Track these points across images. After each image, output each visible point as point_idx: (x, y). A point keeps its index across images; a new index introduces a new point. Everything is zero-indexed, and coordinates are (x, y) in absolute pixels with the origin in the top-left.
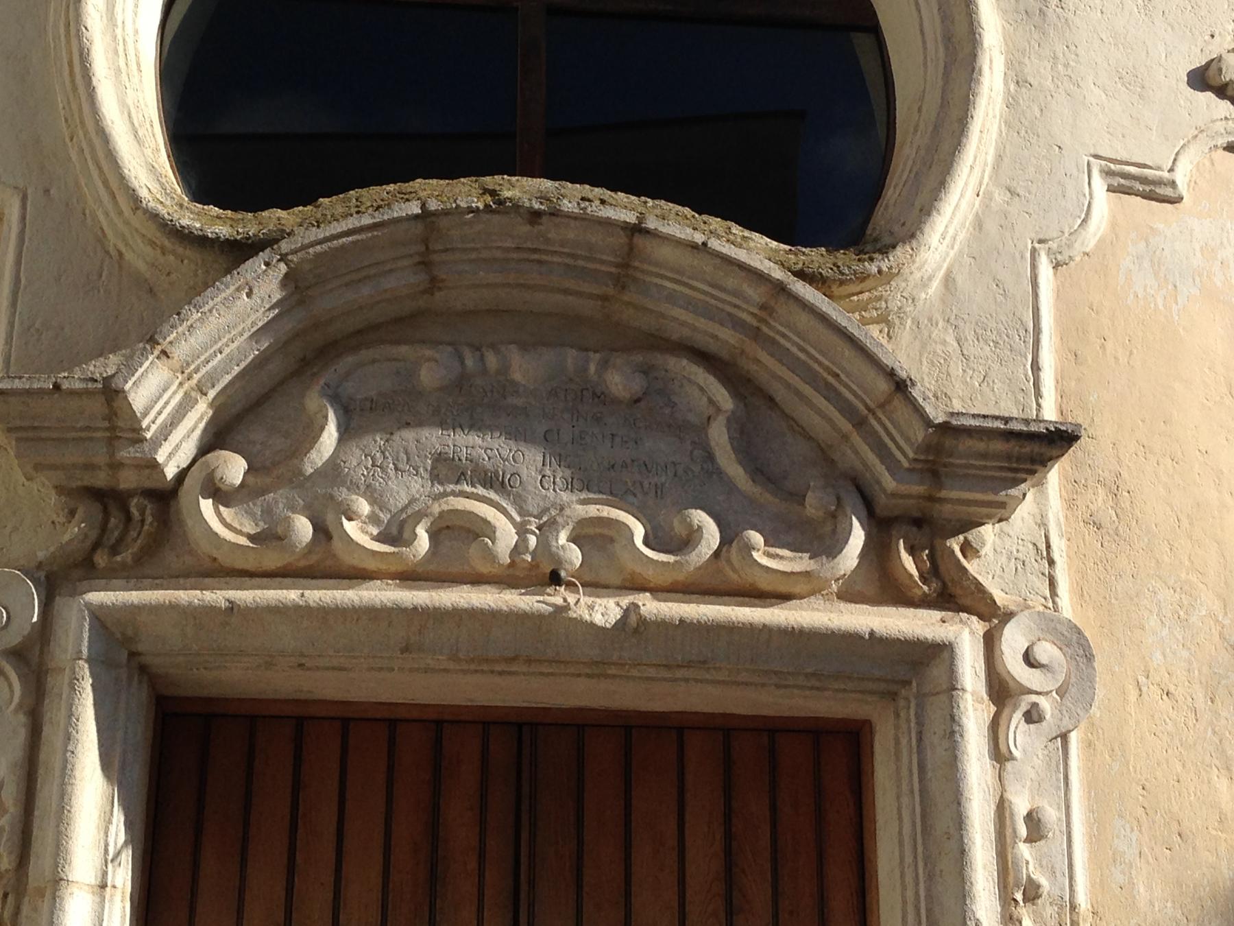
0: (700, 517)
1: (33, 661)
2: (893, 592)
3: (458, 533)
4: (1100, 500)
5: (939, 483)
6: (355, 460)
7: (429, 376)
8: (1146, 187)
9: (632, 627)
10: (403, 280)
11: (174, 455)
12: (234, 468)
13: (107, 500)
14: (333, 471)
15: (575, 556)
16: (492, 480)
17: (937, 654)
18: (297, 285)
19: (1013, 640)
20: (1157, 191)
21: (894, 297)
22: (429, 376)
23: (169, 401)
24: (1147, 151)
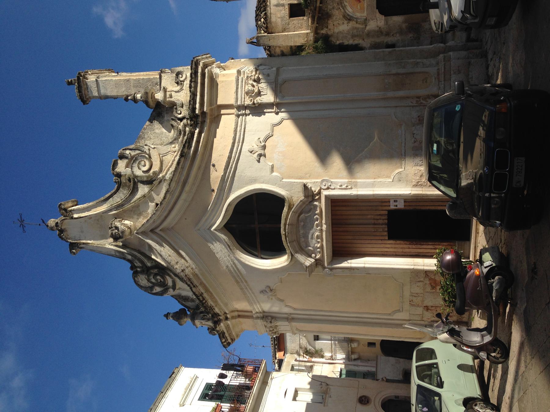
0: (315, 217)
1: (331, 269)
2: (320, 198)
3: (318, 237)
4: (308, 176)
5: (310, 196)
6: (312, 245)
7: (303, 240)
8: (272, 168)
9: (326, 224)
10: (295, 243)
11: (313, 260)
12: (313, 255)
13: (316, 264)
14: (313, 247)
15: (319, 227)
16: (313, 235)
17: (327, 197)
18: (297, 252)
19: (323, 187)
20: (273, 167)
21: (289, 197)
22: (303, 240)
23: (308, 262)
24: (268, 169)
